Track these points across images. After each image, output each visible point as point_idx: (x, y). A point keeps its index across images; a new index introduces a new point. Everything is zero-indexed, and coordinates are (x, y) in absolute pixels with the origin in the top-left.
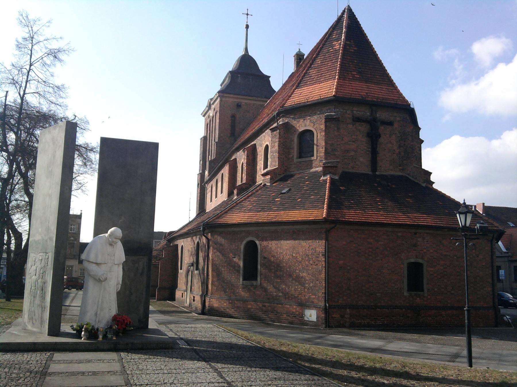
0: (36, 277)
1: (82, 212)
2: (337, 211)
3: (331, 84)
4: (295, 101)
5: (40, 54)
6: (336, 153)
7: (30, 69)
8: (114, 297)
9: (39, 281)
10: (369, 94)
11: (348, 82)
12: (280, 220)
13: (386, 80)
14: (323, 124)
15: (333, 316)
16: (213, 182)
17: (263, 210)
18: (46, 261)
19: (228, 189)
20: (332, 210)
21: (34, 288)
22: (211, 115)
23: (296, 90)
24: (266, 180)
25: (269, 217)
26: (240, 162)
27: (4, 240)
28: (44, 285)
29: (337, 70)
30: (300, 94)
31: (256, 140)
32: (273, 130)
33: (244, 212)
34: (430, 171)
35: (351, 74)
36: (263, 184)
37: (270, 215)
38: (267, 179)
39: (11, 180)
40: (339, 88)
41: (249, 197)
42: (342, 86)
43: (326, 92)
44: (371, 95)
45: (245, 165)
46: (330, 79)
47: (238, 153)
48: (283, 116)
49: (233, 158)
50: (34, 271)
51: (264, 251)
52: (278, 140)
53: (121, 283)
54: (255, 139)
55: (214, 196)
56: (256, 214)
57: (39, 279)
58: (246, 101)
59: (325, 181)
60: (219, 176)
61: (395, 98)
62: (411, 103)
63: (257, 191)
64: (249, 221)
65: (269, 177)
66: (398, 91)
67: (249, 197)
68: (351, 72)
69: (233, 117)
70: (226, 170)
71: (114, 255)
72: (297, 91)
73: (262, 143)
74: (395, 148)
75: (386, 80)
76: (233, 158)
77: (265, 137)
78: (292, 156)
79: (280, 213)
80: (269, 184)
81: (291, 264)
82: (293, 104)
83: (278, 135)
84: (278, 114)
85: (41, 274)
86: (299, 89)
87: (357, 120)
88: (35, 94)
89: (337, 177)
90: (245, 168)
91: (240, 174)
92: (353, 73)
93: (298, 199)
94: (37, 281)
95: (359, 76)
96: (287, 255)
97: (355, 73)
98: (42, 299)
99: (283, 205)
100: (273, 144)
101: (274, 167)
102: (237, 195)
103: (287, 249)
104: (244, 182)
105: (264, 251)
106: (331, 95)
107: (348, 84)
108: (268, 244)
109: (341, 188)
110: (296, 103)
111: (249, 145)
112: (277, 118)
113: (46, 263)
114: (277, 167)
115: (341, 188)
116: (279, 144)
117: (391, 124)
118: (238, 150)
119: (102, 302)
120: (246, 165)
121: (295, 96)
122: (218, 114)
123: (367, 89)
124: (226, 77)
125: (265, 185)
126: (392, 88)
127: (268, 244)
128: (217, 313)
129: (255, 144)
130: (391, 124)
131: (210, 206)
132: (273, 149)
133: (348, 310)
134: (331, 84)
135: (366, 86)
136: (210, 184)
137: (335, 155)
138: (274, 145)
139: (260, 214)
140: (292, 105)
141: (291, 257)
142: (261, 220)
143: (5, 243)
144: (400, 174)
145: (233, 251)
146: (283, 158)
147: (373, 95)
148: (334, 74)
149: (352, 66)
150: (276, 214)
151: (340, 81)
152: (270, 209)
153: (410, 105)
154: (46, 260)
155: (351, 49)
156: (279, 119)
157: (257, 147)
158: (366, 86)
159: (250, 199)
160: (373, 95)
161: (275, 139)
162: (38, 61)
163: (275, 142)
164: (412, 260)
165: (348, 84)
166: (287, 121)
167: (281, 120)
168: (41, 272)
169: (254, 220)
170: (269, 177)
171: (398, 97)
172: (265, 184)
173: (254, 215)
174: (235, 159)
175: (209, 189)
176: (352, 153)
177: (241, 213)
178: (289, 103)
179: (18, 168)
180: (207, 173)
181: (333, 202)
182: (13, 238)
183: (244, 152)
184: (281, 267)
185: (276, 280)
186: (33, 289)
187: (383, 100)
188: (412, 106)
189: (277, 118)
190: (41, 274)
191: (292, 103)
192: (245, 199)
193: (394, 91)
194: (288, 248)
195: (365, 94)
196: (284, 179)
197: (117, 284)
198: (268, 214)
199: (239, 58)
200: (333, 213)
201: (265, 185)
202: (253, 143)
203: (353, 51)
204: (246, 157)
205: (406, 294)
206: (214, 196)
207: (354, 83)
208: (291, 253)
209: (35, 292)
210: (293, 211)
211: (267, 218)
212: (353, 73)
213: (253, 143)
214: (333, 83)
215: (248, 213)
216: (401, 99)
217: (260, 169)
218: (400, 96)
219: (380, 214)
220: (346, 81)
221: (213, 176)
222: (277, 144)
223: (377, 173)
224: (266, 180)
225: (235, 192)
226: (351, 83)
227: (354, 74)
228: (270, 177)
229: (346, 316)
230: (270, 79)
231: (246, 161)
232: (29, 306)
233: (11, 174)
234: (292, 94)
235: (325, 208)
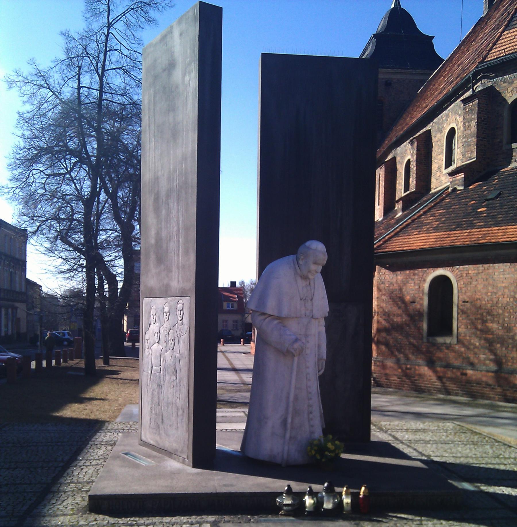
0: (160, 347)
4: (506, 50)
5: (121, 10)
7: (108, 33)
8: (314, 386)
9: (168, 354)
12: (494, 240)
14: (434, 142)
17: (459, 226)
18: (179, 316)
19: (384, 204)
21: (158, 368)
23: (506, 32)
24: (456, 182)
25: (473, 236)
26: (403, 162)
27: (95, 284)
28: (178, 363)
30: (514, 38)
31: (431, 124)
32: (465, 101)
33: (427, 231)
36: (450, 190)
37: (473, 235)
38: (459, 180)
39: (96, 198)
41: (430, 209)
45: (415, 164)
47: (398, 148)
48: (484, 77)
49: (389, 157)
50: (156, 335)
51: (463, 291)
52: (476, 116)
53: (325, 357)
54: (429, 123)
56: (448, 234)
57: (166, 351)
58: (399, 77)
63: (444, 199)
64: (438, 244)
65: (461, 176)
67: (430, 209)
71: (312, 300)
72: (508, 34)
73: (443, 127)
76: (389, 157)
77: (447, 116)
78: (499, 140)
79: (491, 230)
80: (462, 188)
81: (511, 311)
82: (502, 55)
83: (477, 109)
84: (475, 75)
85: (170, 342)
86: (511, 31)
88: (118, 70)
90: (415, 169)
91: (402, 179)
94: (162, 354)
96: (505, 296)
98: (176, 391)
99: (493, 217)
100: (467, 124)
101: (469, 160)
102: (403, 210)
103: (505, 287)
104: (413, 188)
105: (463, 291)
108: (471, 280)
110: (507, 53)
111: (419, 134)
112: (472, 82)
113: (180, 319)
114: (475, 159)
116: (477, 122)
118: (398, 143)
119: (296, 398)
120: (416, 164)
121: (504, 42)
124: (369, 44)
125: (455, 190)
127: (471, 280)
128: (387, 382)
129: (429, 131)
132: (467, 131)
138: (469, 126)
139: (455, 234)
140: (499, 57)
141: (512, 300)
142: (459, 243)
143: (97, 287)
145: (411, 292)
146: (484, 145)
150: (484, 232)
152: (472, 226)
154: (178, 313)
156: (476, 83)
157: (433, 134)
159: (433, 211)
161: (470, 115)
162: (119, 20)
163: (471, 121)
166: (490, 84)
167: (479, 84)
168: (171, 337)
169: (447, 242)
170: (461, 176)
172: (456, 188)
173: (446, 236)
174: (394, 159)
177: (422, 234)
178: (494, 55)
179: (104, 186)
182: (106, 282)
184: (494, 315)
185: (484, 336)
186: (156, 371)
189: (472, 82)
190: (170, 342)
191: (500, 54)
192: (425, 213)
194: (507, 285)
196: (485, 177)
197: (319, 360)
198: (470, 232)
199: (386, 15)
201: (455, 190)
202: (424, 130)
204: (415, 152)
208: (512, 294)
209: (160, 377)
210: (513, 225)
211: (470, 238)
213: (424, 130)
215: (435, 233)
217: (439, 168)
222: (474, 124)
224: (456, 182)
225: (398, 206)
228: (463, 176)
230: (433, 41)
231: (415, 157)
232: (150, 402)
233: (94, 194)
234: (498, 40)
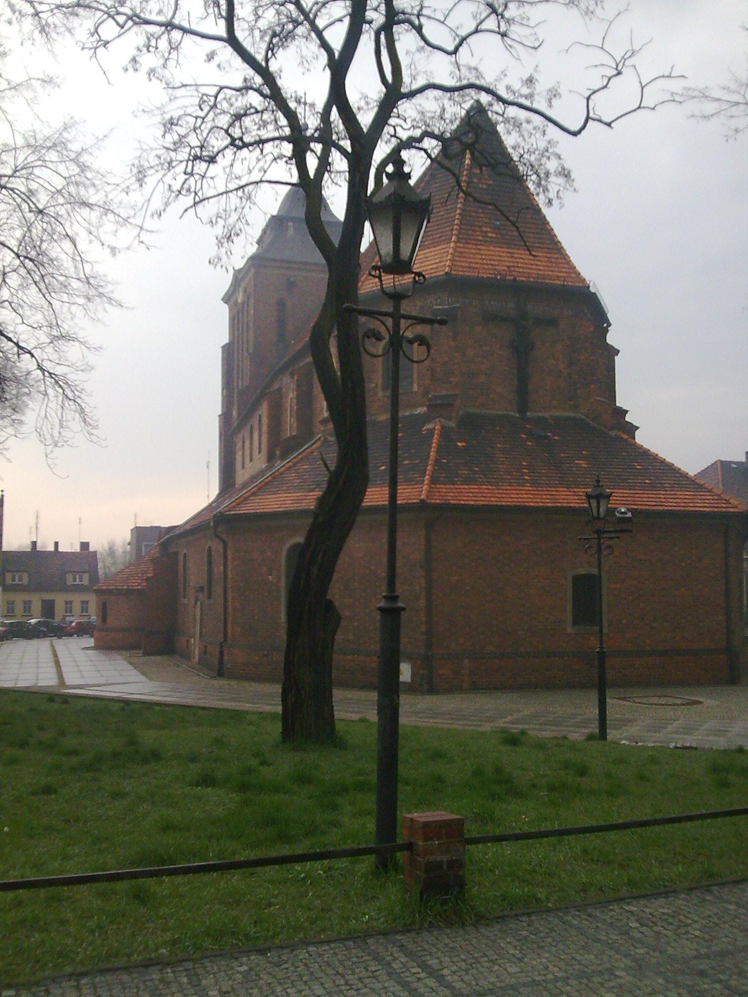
1: (4, 493)
2: (447, 486)
3: (443, 251)
6: (452, 379)
10: (513, 269)
11: (474, 246)
13: (547, 242)
15: (440, 672)
16: (246, 432)
20: (438, 486)
22: (239, 301)
29: (453, 225)
34: (625, 408)
35: (482, 231)
40: (457, 259)
42: (464, 255)
43: (434, 266)
44: (516, 269)
46: (440, 243)
49: (276, 386)
55: (247, 459)
59: (431, 432)
60: (255, 421)
61: (562, 274)
62: (591, 285)
66: (569, 262)
68: (480, 227)
69: (281, 304)
70: (264, 410)
74: (562, 366)
75: (547, 242)
76: (276, 386)
87: (490, 318)
89: (453, 424)
92: (484, 229)
93: (381, 466)
95: (496, 234)
97: (489, 230)
106: (441, 273)
107: (474, 251)
109: (459, 444)
115: (459, 444)
117: (553, 322)
122: (252, 301)
123: (510, 260)
126: (556, 256)
130: (553, 322)
131: (242, 476)
133: (466, 661)
134: (443, 251)
135: (508, 252)
136: (240, 436)
137: (450, 382)
144: (571, 414)
147: (521, 270)
148: (449, 233)
149: (482, 215)
151: (458, 245)
153: (589, 287)
155: (482, 183)
158: (508, 252)
160: (521, 270)
164: (582, 571)
165: (474, 251)
171: (567, 273)
174: (280, 390)
175: (240, 445)
176: (482, 379)
180: (234, 413)
181: (442, 471)
183: (292, 377)
187: (538, 278)
188: (592, 290)
193: (560, 261)
195: (505, 268)
200: (440, 490)
203: (485, 186)
205: (570, 630)
206: (247, 459)
207: (485, 248)
212: (484, 229)
214: (446, 250)
216: (573, 275)
218: (571, 271)
219: (525, 490)
220: (470, 246)
221: (246, 417)
223: (528, 414)
226: (480, 249)
227: (486, 232)
229: (463, 672)
235: (426, 482)
